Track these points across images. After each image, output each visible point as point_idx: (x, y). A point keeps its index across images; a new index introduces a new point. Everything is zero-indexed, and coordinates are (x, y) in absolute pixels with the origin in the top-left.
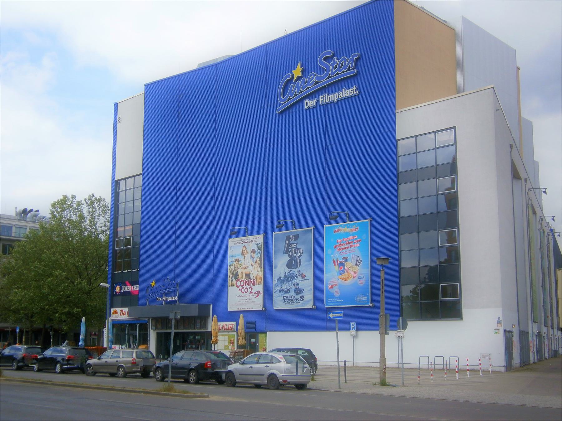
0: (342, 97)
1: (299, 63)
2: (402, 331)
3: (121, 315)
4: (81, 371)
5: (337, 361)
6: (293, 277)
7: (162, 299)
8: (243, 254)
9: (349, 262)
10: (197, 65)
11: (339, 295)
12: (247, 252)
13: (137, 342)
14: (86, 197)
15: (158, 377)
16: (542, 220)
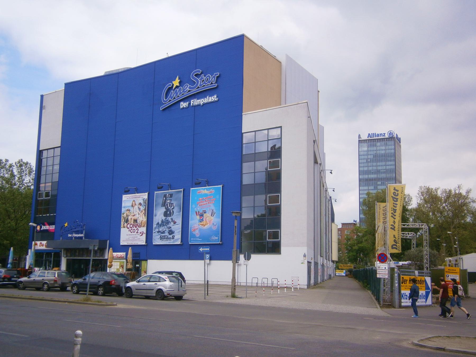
0: (206, 102)
1: (178, 76)
2: (247, 261)
3: (40, 246)
4: (13, 286)
5: (204, 280)
6: (168, 222)
7: (72, 235)
8: (132, 206)
9: (207, 214)
10: (104, 72)
11: (199, 235)
12: (135, 204)
13: (52, 265)
14: (17, 161)
15: (100, 293)
16: (327, 191)
